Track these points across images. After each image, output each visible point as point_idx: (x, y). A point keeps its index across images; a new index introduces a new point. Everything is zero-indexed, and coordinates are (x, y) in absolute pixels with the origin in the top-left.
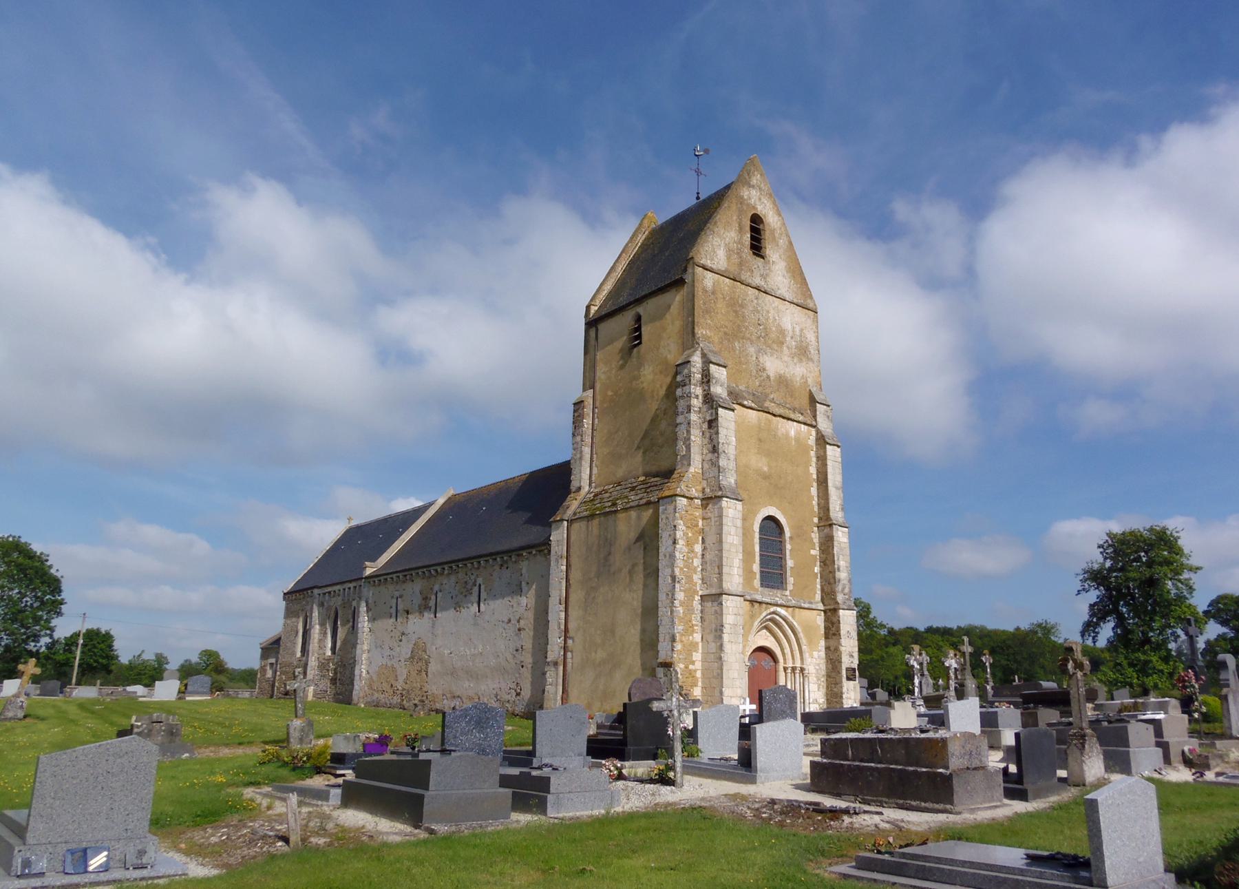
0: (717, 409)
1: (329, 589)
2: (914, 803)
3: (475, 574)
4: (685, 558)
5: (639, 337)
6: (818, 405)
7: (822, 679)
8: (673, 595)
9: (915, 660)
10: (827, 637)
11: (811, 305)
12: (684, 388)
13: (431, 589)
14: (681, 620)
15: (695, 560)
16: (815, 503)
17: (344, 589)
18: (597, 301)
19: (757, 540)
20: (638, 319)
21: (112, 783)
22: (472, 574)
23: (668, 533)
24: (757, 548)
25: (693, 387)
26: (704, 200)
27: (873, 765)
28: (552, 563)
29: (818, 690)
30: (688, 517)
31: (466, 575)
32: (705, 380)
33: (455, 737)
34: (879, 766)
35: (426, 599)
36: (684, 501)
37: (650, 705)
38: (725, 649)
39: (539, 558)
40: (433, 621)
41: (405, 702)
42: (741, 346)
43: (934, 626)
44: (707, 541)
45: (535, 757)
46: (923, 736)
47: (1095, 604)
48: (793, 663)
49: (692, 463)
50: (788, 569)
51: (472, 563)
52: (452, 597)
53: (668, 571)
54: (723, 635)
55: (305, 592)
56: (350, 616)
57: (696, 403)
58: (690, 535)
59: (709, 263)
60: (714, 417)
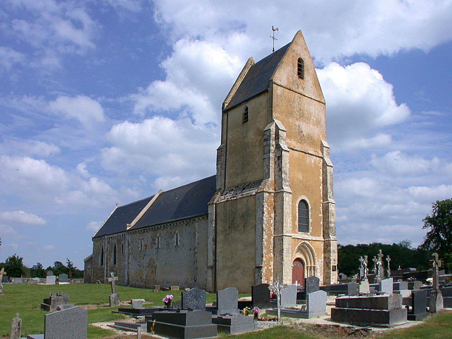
0: (282, 151)
1: (111, 236)
2: (382, 325)
3: (175, 229)
4: (267, 220)
5: (247, 117)
6: (324, 148)
8: (263, 236)
9: (365, 262)
10: (324, 252)
11: (323, 101)
12: (267, 142)
13: (156, 236)
14: (266, 248)
15: (271, 220)
16: (321, 193)
17: (118, 236)
18: (228, 101)
19: (297, 211)
20: (247, 109)
21: (72, 325)
22: (173, 229)
23: (260, 209)
24: (297, 215)
25: (271, 141)
26: (276, 51)
27: (357, 309)
28: (209, 223)
29: (321, 276)
30: (269, 201)
31: (171, 229)
32: (277, 138)
33: (187, 303)
34: (360, 309)
35: (154, 240)
36: (267, 194)
37: (268, 288)
38: (284, 260)
39: (203, 221)
40: (157, 250)
41: (147, 285)
42: (292, 121)
43: (352, 245)
44: (277, 212)
45: (218, 310)
46: (378, 296)
47: (430, 233)
48: (311, 265)
49: (270, 176)
50: (310, 223)
51: (174, 224)
52: (165, 239)
53: (260, 226)
54: (284, 254)
55: (101, 237)
56: (121, 248)
57: (272, 148)
58: (270, 209)
59: (279, 83)
60: (280, 155)
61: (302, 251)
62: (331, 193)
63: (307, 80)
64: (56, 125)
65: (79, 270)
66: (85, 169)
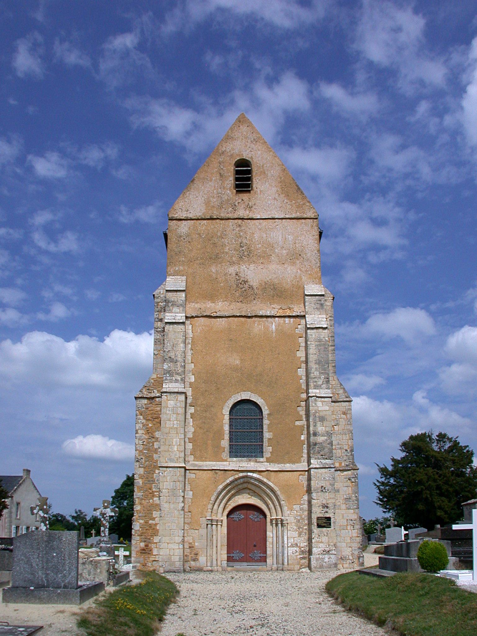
7: (305, 528)
24: (226, 428)
61: (255, 492)
62: (320, 378)
63: (261, 191)
64: (379, 351)
65: (131, 525)
66: (423, 398)
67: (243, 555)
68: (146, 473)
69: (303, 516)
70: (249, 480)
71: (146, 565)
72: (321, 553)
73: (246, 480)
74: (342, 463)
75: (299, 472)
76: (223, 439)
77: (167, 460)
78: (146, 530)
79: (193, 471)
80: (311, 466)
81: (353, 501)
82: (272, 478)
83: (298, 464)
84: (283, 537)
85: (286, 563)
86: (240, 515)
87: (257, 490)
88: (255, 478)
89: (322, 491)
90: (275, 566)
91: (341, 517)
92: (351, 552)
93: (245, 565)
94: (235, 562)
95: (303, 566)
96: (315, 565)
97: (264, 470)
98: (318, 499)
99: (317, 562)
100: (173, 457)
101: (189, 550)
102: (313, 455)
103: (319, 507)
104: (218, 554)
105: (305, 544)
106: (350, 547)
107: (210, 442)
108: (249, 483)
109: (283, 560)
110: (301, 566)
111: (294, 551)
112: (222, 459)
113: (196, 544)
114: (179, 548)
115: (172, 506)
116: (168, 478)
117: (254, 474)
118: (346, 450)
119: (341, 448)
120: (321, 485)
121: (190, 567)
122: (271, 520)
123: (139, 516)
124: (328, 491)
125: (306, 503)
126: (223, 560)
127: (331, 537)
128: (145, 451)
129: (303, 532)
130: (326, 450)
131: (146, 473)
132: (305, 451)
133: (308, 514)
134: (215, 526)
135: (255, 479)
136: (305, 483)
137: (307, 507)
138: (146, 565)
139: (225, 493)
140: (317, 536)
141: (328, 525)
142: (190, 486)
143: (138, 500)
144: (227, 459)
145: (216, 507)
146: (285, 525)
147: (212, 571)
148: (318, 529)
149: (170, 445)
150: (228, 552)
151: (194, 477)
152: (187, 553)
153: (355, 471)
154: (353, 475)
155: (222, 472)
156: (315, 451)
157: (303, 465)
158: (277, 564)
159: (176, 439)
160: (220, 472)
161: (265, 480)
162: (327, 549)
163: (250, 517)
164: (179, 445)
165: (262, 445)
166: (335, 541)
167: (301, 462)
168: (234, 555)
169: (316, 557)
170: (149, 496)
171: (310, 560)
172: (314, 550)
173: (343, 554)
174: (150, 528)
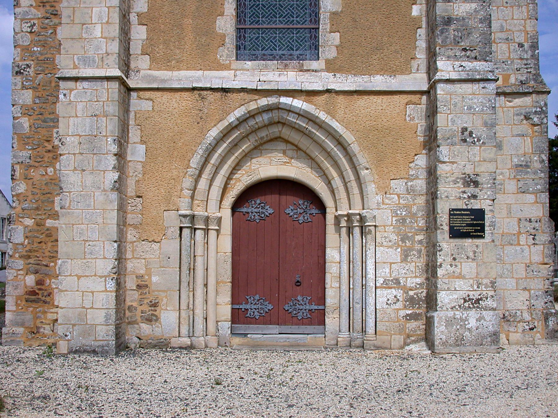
61: (298, 149)
67: (270, 307)
68: (37, 101)
69: (414, 210)
70: (283, 118)
71: (38, 332)
72: (460, 306)
73: (275, 115)
74: (510, 75)
75: (405, 96)
76: (222, 14)
77: (76, 60)
78: (40, 243)
79: (148, 94)
80: (438, 76)
81: (535, 173)
82: (339, 111)
83: (403, 76)
84: (363, 262)
85: (370, 329)
86: (263, 208)
87: (304, 143)
88: (298, 111)
89: (465, 141)
90: (344, 336)
91: (504, 213)
92: (528, 303)
93: (274, 332)
94: (251, 323)
95: (413, 338)
96: (444, 337)
97: (321, 88)
98: (453, 163)
99: (450, 329)
100: (91, 53)
101: (136, 295)
102: (443, 49)
103: (455, 182)
104: (209, 303)
105: (418, 280)
106: (525, 289)
107: (188, 21)
108: (284, 124)
109: (363, 322)
110: (408, 336)
111: (391, 297)
112: (218, 63)
113: (154, 279)
114: (106, 291)
115: (89, 179)
116: (80, 107)
117: (295, 100)
118: (521, 45)
119: (507, 39)
120: (460, 124)
121: (140, 339)
122: (337, 219)
123: (23, 209)
124: (479, 140)
125: (423, 175)
126: (223, 318)
127: (484, 263)
128: (35, 49)
129: (413, 250)
130: (476, 37)
131: (37, 101)
132: (422, 44)
133: (427, 201)
134: (203, 232)
135: (299, 115)
136: (421, 124)
137: (424, 187)
138: (38, 332)
139: (225, 148)
140: (449, 259)
141: (476, 231)
142: (139, 132)
143: (20, 169)
144: (230, 63)
145: (203, 184)
146: (370, 231)
147: (191, 347)
148: (452, 240)
149: (83, 24)
150: (235, 299)
151: (151, 109)
152: (131, 301)
153: (542, 97)
154: (536, 107)
155: (218, 95)
156: (447, 38)
157: (415, 79)
158: (349, 331)
159: (98, 9)
160: (211, 97)
161: (322, 116)
162: (475, 295)
163: (287, 211)
164: (107, 22)
165: (318, 28)
166: (493, 275)
167: (411, 73)
168: (248, 307)
169: (446, 316)
170: (46, 159)
171: (429, 323)
172: (443, 297)
173: (509, 306)
174: (47, 239)
